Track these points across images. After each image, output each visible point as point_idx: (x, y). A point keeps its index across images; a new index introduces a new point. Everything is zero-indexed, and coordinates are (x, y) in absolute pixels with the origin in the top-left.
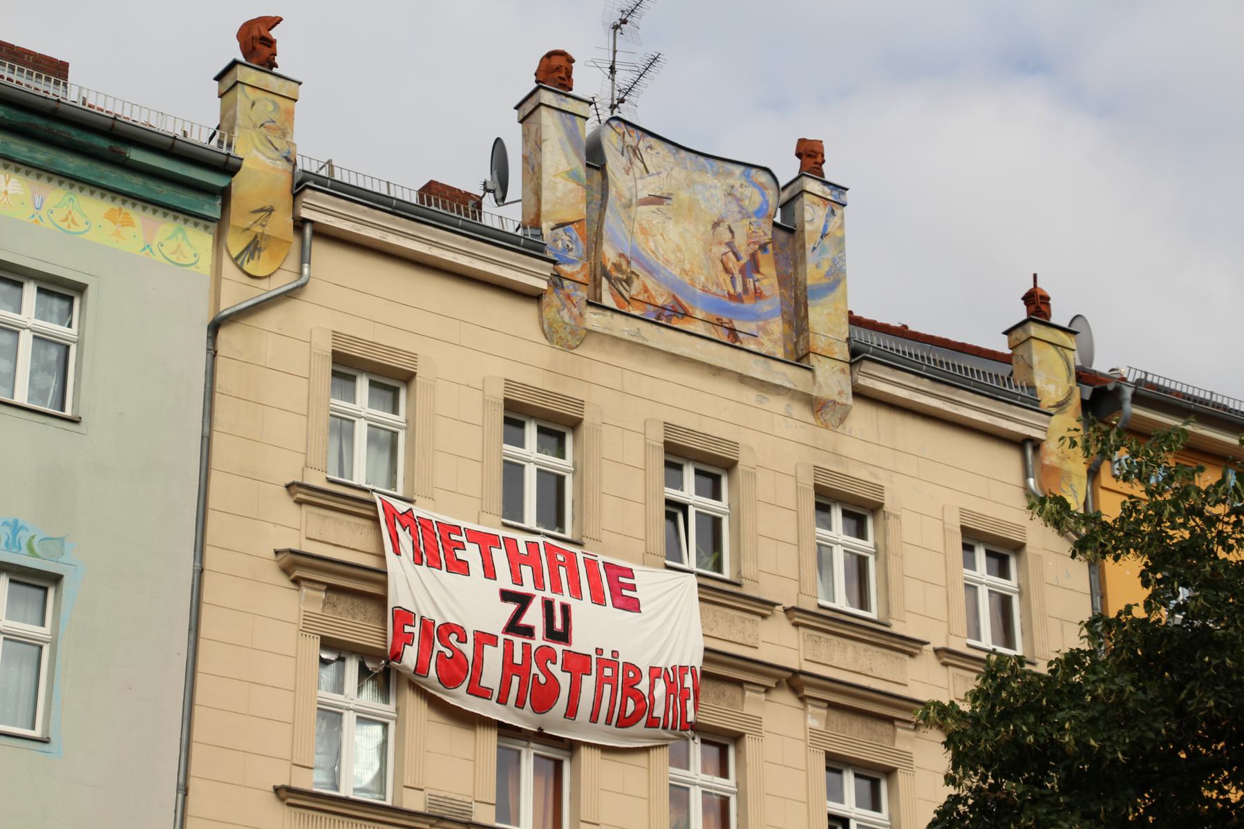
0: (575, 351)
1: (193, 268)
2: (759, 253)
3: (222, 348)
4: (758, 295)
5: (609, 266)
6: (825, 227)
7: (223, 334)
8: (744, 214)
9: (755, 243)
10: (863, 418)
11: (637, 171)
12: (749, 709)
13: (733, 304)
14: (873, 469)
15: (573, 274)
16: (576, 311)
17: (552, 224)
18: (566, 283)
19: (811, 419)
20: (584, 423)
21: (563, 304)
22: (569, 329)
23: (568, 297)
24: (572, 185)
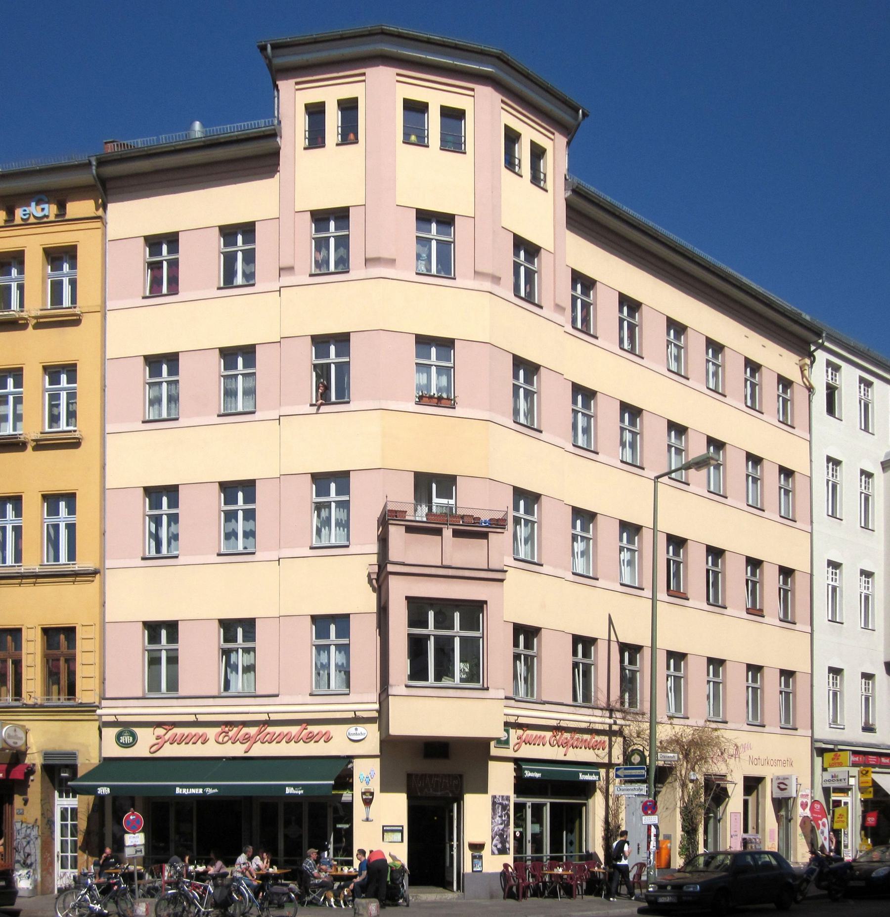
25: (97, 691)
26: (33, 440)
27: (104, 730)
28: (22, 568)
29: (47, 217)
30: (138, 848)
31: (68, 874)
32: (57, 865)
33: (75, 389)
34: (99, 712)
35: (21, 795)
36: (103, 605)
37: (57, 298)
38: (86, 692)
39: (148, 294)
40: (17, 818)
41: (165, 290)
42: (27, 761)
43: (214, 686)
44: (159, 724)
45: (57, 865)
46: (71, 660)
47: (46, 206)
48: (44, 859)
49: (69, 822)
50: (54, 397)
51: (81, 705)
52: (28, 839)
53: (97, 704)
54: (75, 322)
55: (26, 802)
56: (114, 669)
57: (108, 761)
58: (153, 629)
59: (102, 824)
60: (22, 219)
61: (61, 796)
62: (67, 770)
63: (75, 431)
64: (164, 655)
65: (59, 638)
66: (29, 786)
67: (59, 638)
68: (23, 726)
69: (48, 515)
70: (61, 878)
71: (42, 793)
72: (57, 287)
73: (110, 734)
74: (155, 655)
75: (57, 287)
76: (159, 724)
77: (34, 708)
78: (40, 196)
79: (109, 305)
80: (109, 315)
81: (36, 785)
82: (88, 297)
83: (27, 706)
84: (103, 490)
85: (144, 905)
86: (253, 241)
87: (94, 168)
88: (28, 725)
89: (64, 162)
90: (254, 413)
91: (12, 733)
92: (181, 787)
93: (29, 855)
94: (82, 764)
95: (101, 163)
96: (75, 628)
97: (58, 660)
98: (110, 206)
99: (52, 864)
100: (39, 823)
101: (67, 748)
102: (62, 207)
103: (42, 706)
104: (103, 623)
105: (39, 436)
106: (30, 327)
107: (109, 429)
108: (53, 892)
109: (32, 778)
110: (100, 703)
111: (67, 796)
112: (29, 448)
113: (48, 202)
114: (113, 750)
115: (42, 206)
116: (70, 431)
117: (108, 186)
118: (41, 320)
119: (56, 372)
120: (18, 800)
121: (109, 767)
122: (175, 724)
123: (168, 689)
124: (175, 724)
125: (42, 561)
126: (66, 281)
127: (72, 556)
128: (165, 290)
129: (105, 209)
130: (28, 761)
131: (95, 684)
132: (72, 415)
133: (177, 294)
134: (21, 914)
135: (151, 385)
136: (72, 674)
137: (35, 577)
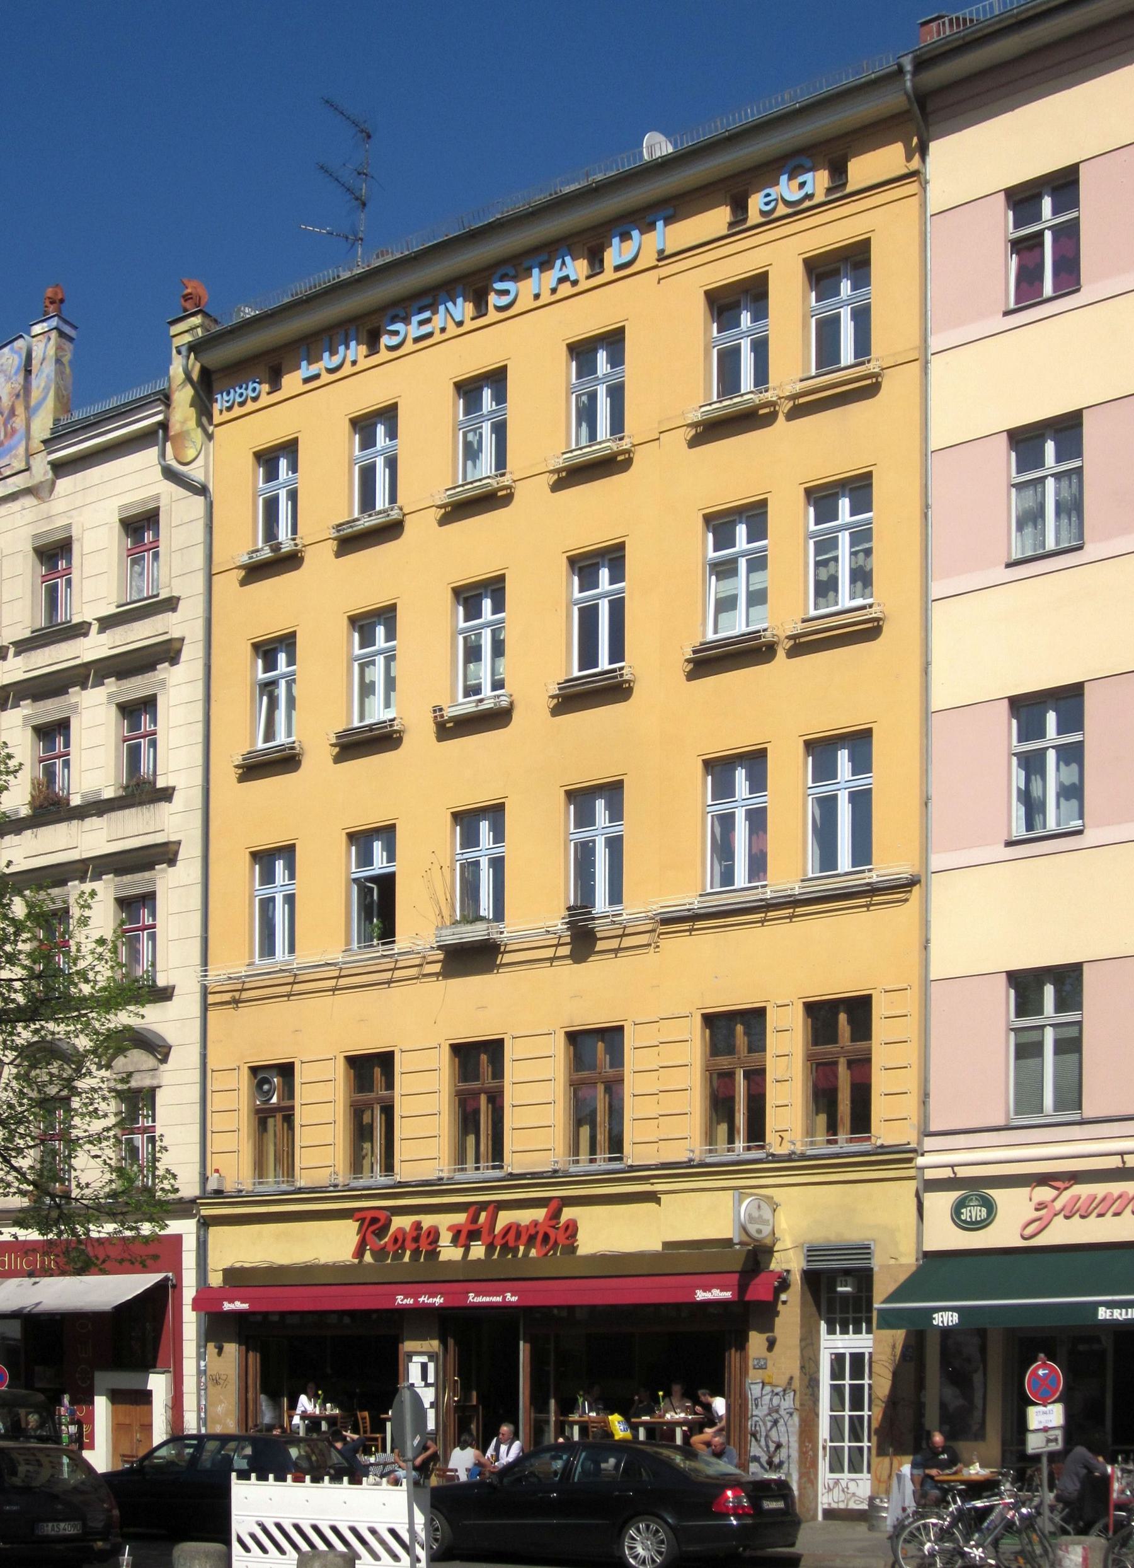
10: (64, 484)
25: (915, 1120)
26: (789, 638)
27: (930, 1198)
28: (768, 890)
29: (809, 197)
30: (1052, 1434)
31: (843, 1483)
32: (823, 1465)
33: (764, 549)
34: (920, 1161)
35: (762, 1331)
36: (926, 945)
37: (828, 353)
38: (891, 1121)
39: (1012, 306)
40: (754, 1375)
41: (1048, 289)
42: (773, 1266)
43: (997, 1103)
44: (1043, 1179)
45: (823, 1465)
46: (862, 1065)
47: (808, 177)
48: (803, 1453)
49: (847, 1382)
50: (826, 546)
51: (883, 1149)
52: (775, 1416)
53: (913, 1145)
54: (869, 389)
55: (771, 1344)
56: (948, 1074)
57: (933, 1259)
58: (1026, 985)
59: (920, 1384)
60: (763, 213)
61: (832, 1331)
62: (850, 1280)
63: (871, 606)
64: (1049, 1036)
65: (841, 1021)
66: (777, 1313)
67: (841, 1021)
68: (769, 1199)
69: (261, 884)
70: (830, 1490)
71: (802, 1327)
72: (828, 330)
73: (940, 1203)
74: (1033, 1036)
75: (828, 330)
76: (1043, 1179)
77: (792, 1162)
78: (794, 162)
79: (935, 344)
80: (936, 363)
81: (791, 1309)
82: (891, 335)
83: (775, 1158)
84: (927, 714)
85: (1079, 1550)
86: (1075, 204)
87: (908, 77)
88: (777, 1194)
89: (848, 80)
90: (1080, 548)
91: (756, 1214)
92: (1110, 1305)
93: (779, 1446)
94: (881, 1267)
95: (921, 65)
96: (869, 997)
97: (836, 1063)
98: (934, 147)
99: (814, 1464)
100: (796, 1384)
101: (853, 1236)
102: (839, 172)
103: (804, 1157)
104: (926, 983)
105: (800, 628)
106: (781, 418)
107: (936, 591)
108: (815, 1517)
109: (783, 1297)
110: (920, 1143)
111: (845, 1331)
112: (781, 653)
113: (813, 169)
114: (944, 1235)
115: (801, 179)
116: (863, 608)
117: (930, 107)
118: (802, 400)
119: (592, 565)
120: (756, 1341)
121: (939, 1270)
122: (1076, 1177)
123: (1059, 1106)
124: (1076, 1177)
125: (704, 888)
126: (846, 314)
127: (862, 853)
128: (1048, 289)
129: (923, 151)
130: (776, 1264)
131: (909, 1106)
132: (862, 577)
133: (1078, 290)
134: (802, 1563)
135: (1019, 486)
136: (616, 1112)
137: (792, 904)
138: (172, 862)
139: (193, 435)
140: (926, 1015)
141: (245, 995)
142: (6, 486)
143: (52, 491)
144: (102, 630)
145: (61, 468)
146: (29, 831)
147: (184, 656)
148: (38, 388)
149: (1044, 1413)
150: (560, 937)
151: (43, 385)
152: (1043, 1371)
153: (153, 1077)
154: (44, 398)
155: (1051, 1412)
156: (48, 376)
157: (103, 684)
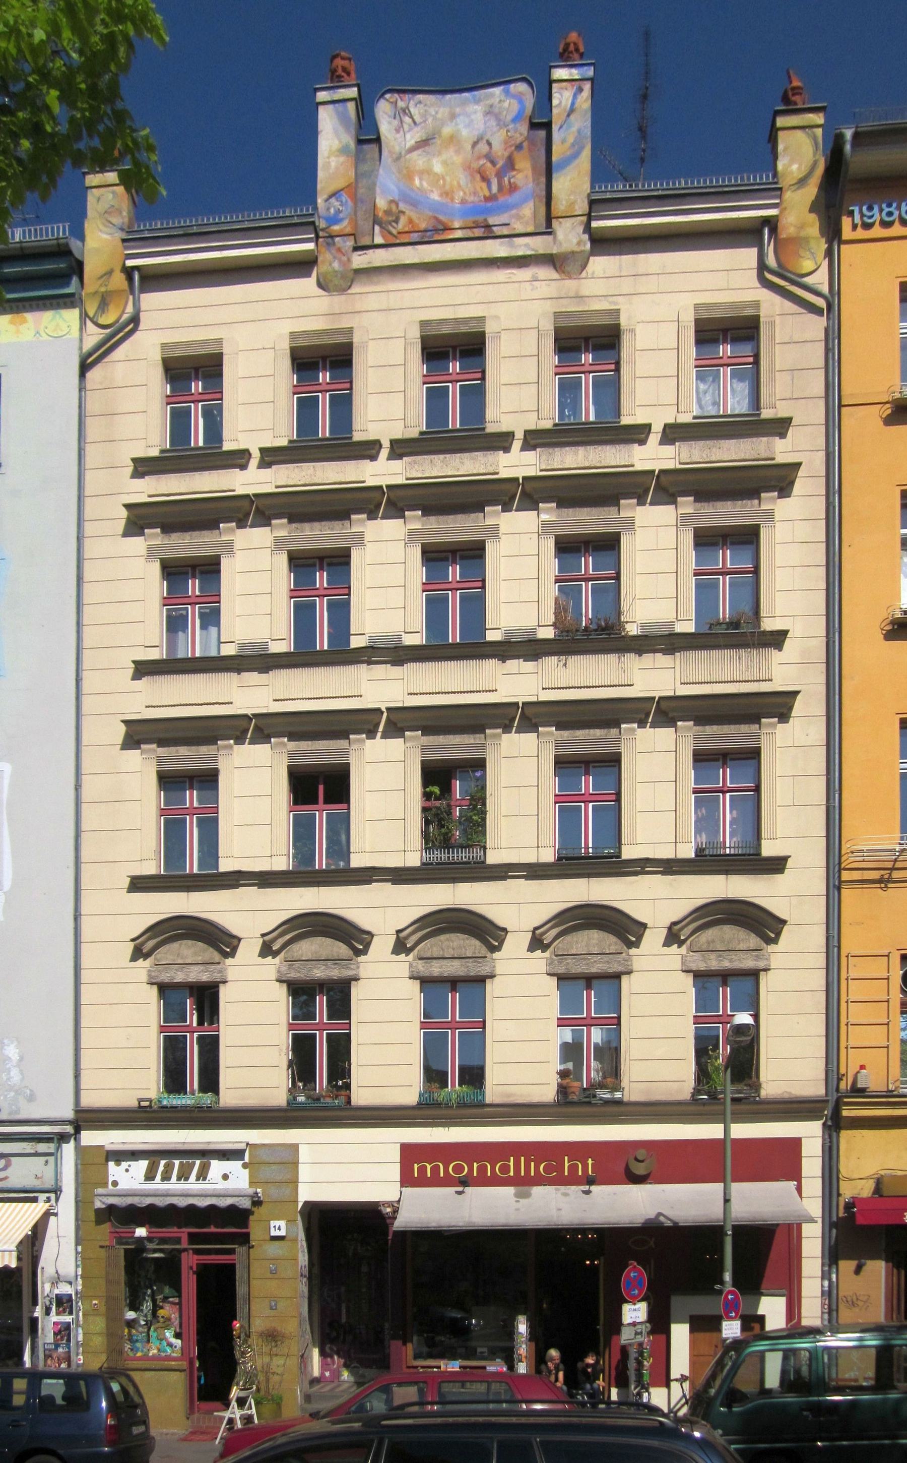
0: (349, 291)
1: (68, 336)
2: (515, 153)
3: (89, 385)
4: (513, 188)
5: (380, 214)
6: (573, 104)
7: (89, 375)
8: (501, 124)
9: (511, 146)
10: (600, 264)
11: (406, 127)
12: (489, 521)
13: (489, 204)
14: (611, 299)
15: (342, 230)
16: (345, 259)
17: (325, 197)
18: (337, 239)
19: (555, 275)
20: (354, 345)
21: (335, 258)
22: (339, 276)
23: (339, 250)
24: (342, 159)
138: (784, 716)
139: (813, 244)
140: (442, 981)
141: (896, 875)
142: (512, 246)
143: (584, 266)
144: (265, 464)
145: (603, 243)
146: (554, 659)
147: (799, 487)
148: (563, 141)
149: (634, 1310)
150: (896, 860)
151: (571, 140)
152: (634, 1274)
153: (757, 959)
154: (576, 155)
155: (639, 1310)
156: (579, 131)
157: (143, 534)
